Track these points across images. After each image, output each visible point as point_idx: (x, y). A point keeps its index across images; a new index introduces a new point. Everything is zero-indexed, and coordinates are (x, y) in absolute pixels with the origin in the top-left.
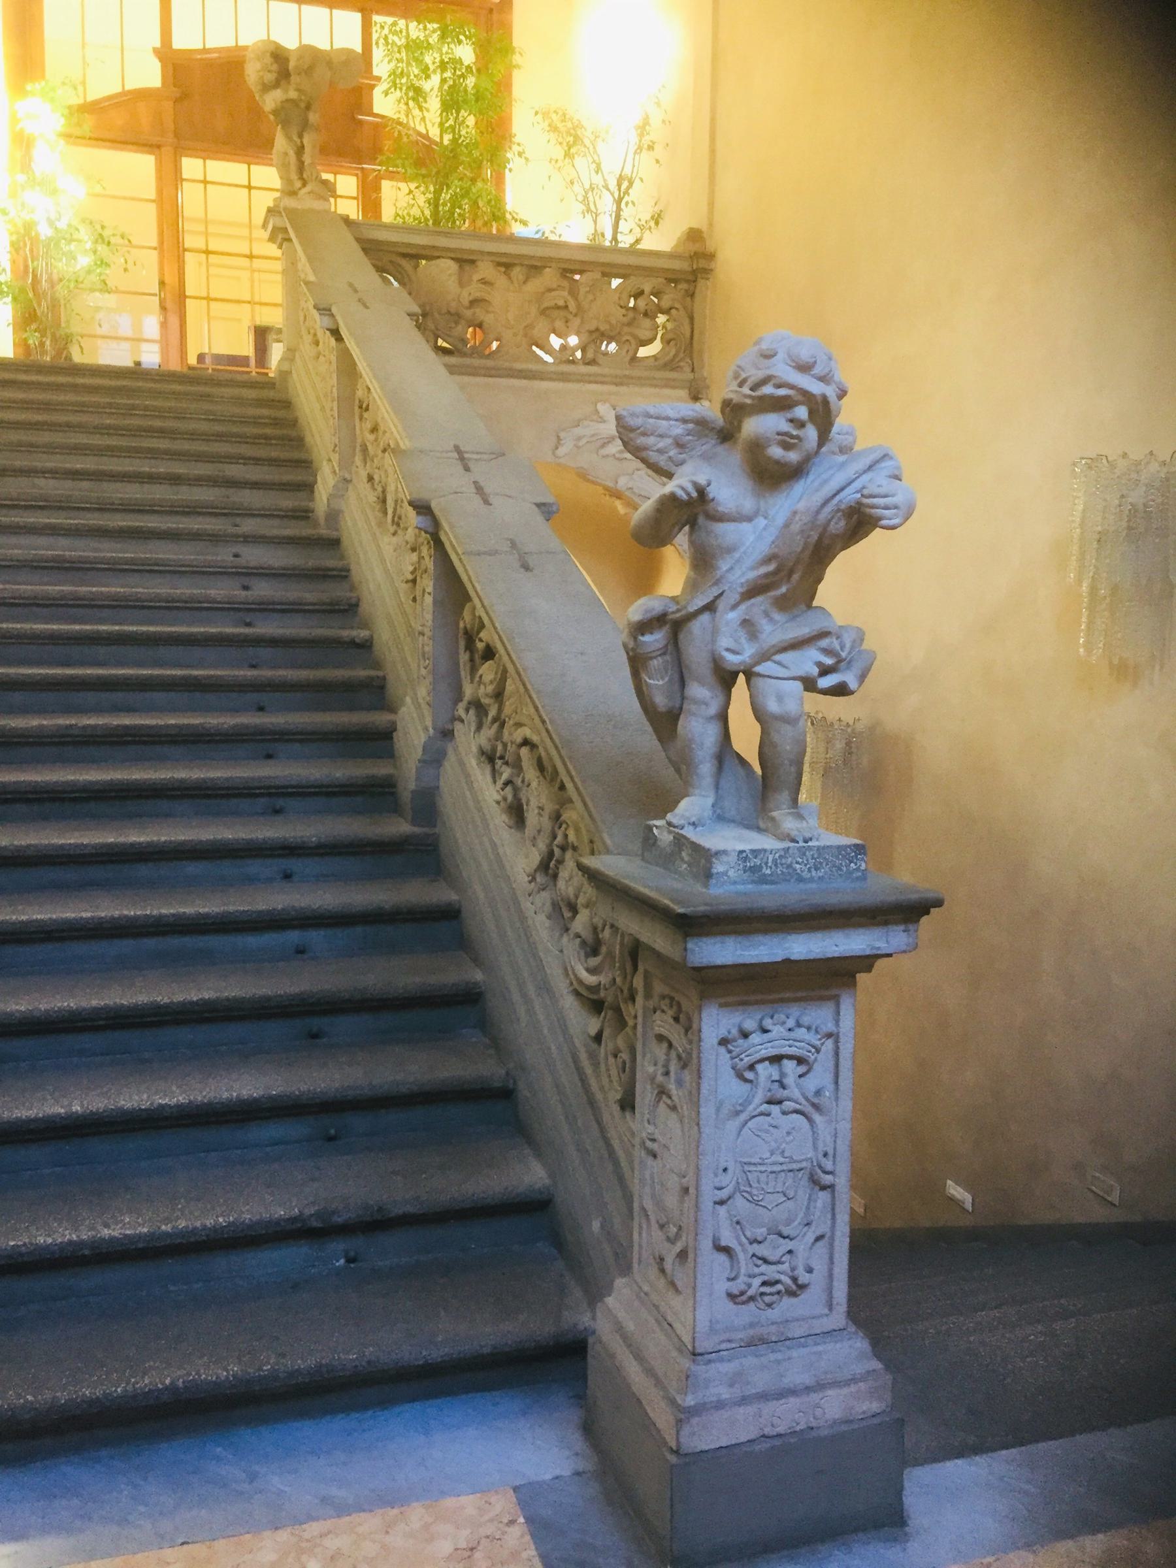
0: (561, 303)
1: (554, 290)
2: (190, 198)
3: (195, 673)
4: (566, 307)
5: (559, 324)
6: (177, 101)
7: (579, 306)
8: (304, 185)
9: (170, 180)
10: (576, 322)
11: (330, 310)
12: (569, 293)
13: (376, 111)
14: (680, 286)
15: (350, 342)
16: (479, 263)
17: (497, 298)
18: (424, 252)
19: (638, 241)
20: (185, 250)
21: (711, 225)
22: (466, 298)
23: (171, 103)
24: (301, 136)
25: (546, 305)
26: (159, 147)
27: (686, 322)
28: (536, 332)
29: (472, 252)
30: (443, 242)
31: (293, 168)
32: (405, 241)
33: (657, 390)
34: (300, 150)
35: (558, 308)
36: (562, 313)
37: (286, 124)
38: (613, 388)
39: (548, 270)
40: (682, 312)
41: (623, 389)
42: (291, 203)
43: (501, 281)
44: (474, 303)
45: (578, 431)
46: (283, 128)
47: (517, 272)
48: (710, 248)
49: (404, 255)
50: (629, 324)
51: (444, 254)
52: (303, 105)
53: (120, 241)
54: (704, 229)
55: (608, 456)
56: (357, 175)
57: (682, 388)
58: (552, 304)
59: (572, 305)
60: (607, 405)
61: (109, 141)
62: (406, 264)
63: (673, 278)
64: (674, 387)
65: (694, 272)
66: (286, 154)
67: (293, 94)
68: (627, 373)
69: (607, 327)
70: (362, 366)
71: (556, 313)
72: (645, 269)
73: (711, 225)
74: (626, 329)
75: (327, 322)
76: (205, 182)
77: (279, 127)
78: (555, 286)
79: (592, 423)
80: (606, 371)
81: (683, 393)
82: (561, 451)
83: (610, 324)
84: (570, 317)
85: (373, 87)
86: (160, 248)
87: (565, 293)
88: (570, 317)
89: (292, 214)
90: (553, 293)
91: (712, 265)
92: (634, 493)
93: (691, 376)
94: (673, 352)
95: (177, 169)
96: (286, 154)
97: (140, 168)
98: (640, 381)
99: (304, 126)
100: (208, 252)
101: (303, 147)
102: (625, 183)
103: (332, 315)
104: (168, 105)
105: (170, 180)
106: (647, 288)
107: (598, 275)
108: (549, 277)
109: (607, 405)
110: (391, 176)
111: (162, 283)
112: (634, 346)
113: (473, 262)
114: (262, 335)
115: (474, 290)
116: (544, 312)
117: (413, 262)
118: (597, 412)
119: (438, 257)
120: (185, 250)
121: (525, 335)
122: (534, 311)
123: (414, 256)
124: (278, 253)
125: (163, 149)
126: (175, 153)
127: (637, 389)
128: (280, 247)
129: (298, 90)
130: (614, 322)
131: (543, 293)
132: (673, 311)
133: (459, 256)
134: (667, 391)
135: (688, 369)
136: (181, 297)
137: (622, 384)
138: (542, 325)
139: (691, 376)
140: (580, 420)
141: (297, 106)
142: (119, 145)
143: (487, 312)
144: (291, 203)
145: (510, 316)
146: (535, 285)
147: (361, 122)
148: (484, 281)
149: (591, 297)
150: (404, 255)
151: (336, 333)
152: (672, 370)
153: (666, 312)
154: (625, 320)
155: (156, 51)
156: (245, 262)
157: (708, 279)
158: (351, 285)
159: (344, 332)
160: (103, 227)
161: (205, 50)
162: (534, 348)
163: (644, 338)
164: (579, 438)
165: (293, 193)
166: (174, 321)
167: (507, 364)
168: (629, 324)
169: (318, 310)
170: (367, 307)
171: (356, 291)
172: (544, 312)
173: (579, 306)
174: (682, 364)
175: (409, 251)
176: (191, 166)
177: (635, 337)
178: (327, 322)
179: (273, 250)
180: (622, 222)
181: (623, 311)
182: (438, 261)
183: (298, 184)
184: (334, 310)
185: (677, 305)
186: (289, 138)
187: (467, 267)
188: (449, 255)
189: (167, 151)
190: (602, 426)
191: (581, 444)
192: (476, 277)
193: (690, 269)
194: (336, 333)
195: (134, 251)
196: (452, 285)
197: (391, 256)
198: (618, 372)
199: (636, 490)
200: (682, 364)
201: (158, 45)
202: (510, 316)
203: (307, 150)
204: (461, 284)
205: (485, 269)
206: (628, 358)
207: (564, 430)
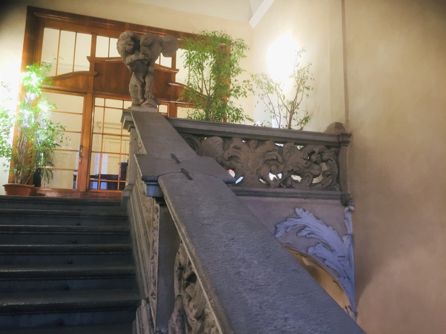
0: (275, 157)
1: (271, 151)
2: (98, 114)
3: (137, 162)
4: (277, 160)
5: (273, 168)
6: (95, 76)
7: (284, 160)
8: (144, 101)
9: (89, 107)
10: (282, 167)
11: (157, 181)
12: (278, 153)
13: (176, 81)
14: (332, 149)
15: (172, 209)
16: (234, 139)
17: (242, 156)
18: (204, 133)
19: (302, 128)
20: (93, 133)
21: (347, 121)
22: (226, 156)
23: (93, 77)
24: (144, 78)
25: (267, 158)
26: (86, 93)
27: (336, 166)
28: (262, 172)
29: (230, 133)
30: (216, 128)
31: (139, 93)
32: (197, 128)
33: (325, 201)
34: (143, 85)
35: (273, 160)
36: (275, 162)
37: (136, 72)
38: (303, 200)
39: (268, 142)
40: (334, 161)
41: (308, 200)
42: (136, 109)
43: (245, 148)
44: (231, 158)
45: (286, 223)
46: (135, 74)
47: (252, 143)
48: (348, 131)
49: (194, 135)
50: (308, 168)
51: (216, 134)
52: (146, 63)
53: (61, 129)
54: (343, 122)
55: (302, 236)
56: (167, 105)
57: (337, 199)
58: (270, 158)
59: (280, 159)
60: (301, 209)
61: (67, 91)
62: (197, 140)
63: (329, 146)
64: (333, 199)
65: (340, 143)
66: (136, 86)
67: (141, 56)
68: (309, 192)
69: (298, 169)
70: (182, 231)
71: (271, 163)
72: (314, 141)
73: (347, 121)
74: (306, 170)
75: (152, 190)
76: (104, 107)
77: (133, 73)
78: (272, 150)
79: (293, 219)
80: (299, 191)
81: (338, 202)
82: (278, 235)
83: (300, 168)
84: (279, 164)
85: (176, 73)
86: (82, 132)
87: (276, 153)
88: (279, 164)
89: (135, 114)
90: (270, 153)
91: (350, 139)
92: (317, 256)
93: (340, 193)
94: (331, 181)
95: (93, 102)
96: (136, 86)
97: (77, 102)
98: (316, 196)
99: (146, 73)
100: (103, 134)
101: (145, 83)
102: (294, 105)
103: (158, 185)
104: (91, 79)
105: (89, 107)
106: (317, 150)
107: (292, 144)
108: (268, 145)
109: (301, 209)
110: (182, 106)
111: (81, 147)
112: (311, 178)
113: (230, 138)
114: (124, 166)
115: (231, 151)
116: (266, 162)
117: (199, 138)
118: (296, 213)
119: (213, 136)
120: (93, 133)
121: (257, 174)
122: (261, 161)
123: (201, 135)
124: (129, 134)
125: (88, 94)
126: (93, 96)
127: (315, 201)
128: (129, 131)
129: (143, 54)
130: (301, 167)
131: (266, 153)
132: (330, 161)
133: (224, 135)
134: (330, 201)
135: (338, 189)
136: (90, 152)
137: (307, 198)
138: (265, 168)
139: (340, 193)
140: (287, 218)
141: (144, 63)
142: (69, 93)
143: (237, 162)
144: (136, 109)
145: (249, 165)
146: (261, 150)
147: (170, 86)
148: (236, 147)
149: (288, 155)
150: (194, 135)
151: (160, 200)
152: (330, 190)
153: (326, 161)
154: (306, 165)
155: (88, 58)
156: (120, 137)
157: (347, 146)
158: (173, 156)
159: (168, 202)
160: (51, 123)
161: (109, 58)
162: (260, 179)
163: (315, 174)
164: (287, 227)
165: (139, 105)
166: (85, 161)
167: (248, 189)
168: (308, 168)
169: (146, 181)
170: (190, 179)
171: (178, 162)
172: (266, 162)
173: (284, 160)
174: (335, 187)
175: (198, 133)
176: (99, 101)
177: (311, 173)
178: (152, 190)
179: (126, 132)
180: (292, 121)
181: (306, 161)
182: (213, 137)
183: (141, 101)
184: (161, 181)
185: (331, 158)
186: (137, 78)
187: (227, 141)
188: (219, 134)
189: (90, 95)
190: (298, 220)
191: (288, 230)
192: (232, 146)
193: (338, 141)
194: (160, 200)
195: (67, 134)
196: (219, 149)
197: (192, 135)
198: (304, 191)
199: (318, 255)
200: (335, 187)
201: (89, 55)
202: (249, 165)
203: (147, 85)
204: (224, 149)
205: (237, 142)
206: (308, 185)
207: (278, 223)
